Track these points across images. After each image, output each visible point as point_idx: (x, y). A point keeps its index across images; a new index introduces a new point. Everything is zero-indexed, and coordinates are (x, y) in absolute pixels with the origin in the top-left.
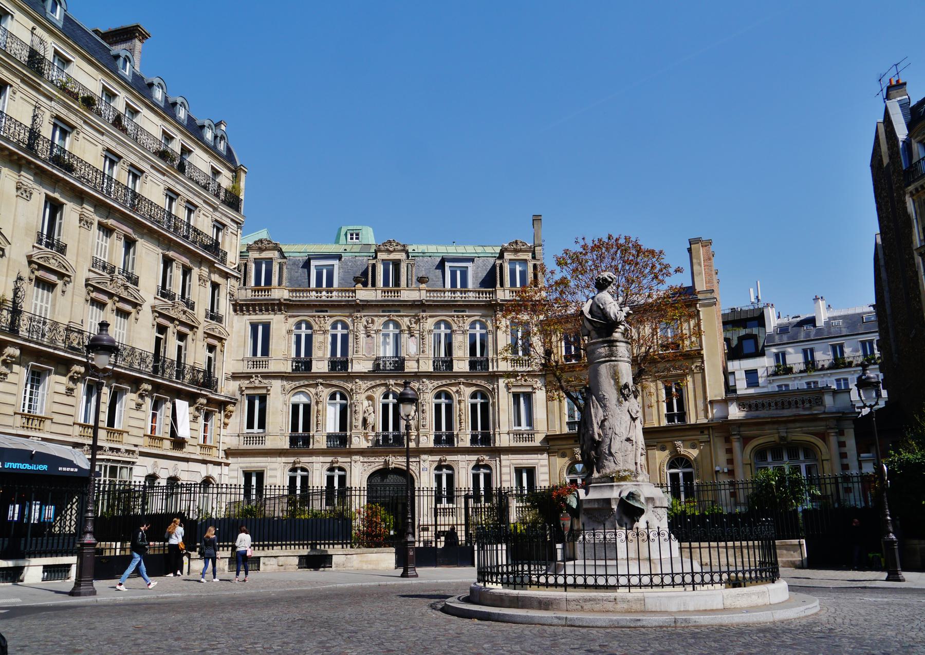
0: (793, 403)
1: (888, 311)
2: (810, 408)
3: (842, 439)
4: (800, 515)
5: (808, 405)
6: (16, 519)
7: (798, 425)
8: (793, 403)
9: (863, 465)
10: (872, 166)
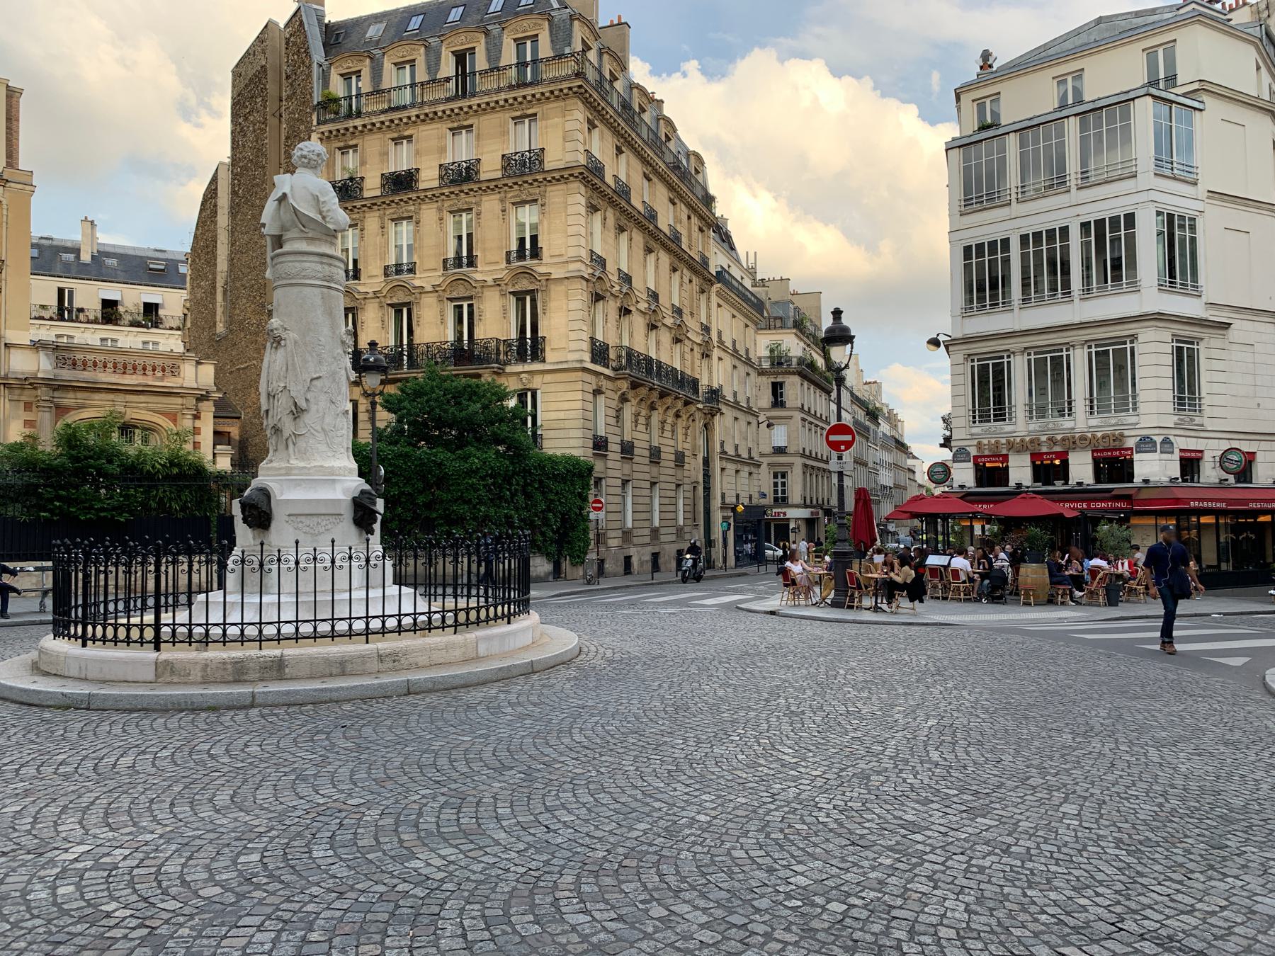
0: (140, 368)
1: (222, 264)
2: (162, 379)
3: (198, 423)
4: (377, 527)
5: (159, 374)
6: (50, 564)
7: (142, 398)
8: (140, 368)
9: (218, 459)
10: (237, 73)
